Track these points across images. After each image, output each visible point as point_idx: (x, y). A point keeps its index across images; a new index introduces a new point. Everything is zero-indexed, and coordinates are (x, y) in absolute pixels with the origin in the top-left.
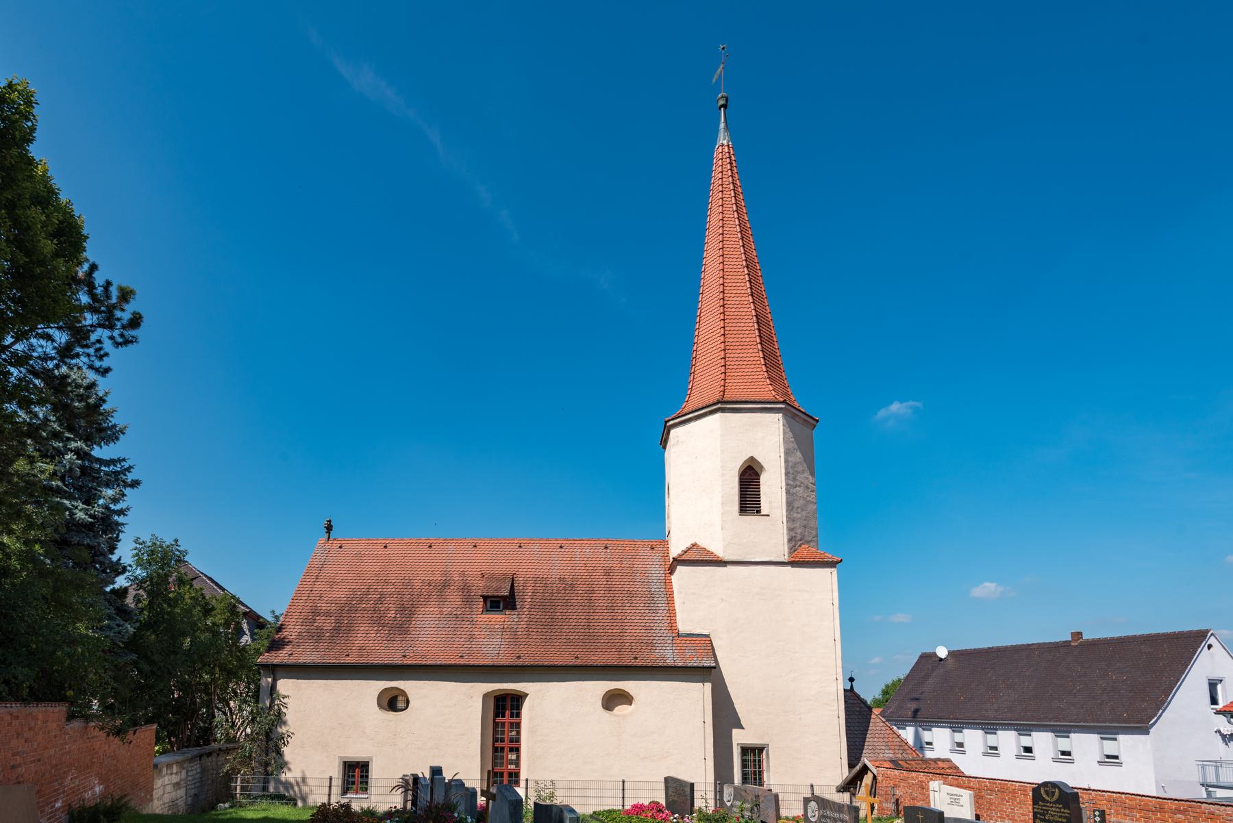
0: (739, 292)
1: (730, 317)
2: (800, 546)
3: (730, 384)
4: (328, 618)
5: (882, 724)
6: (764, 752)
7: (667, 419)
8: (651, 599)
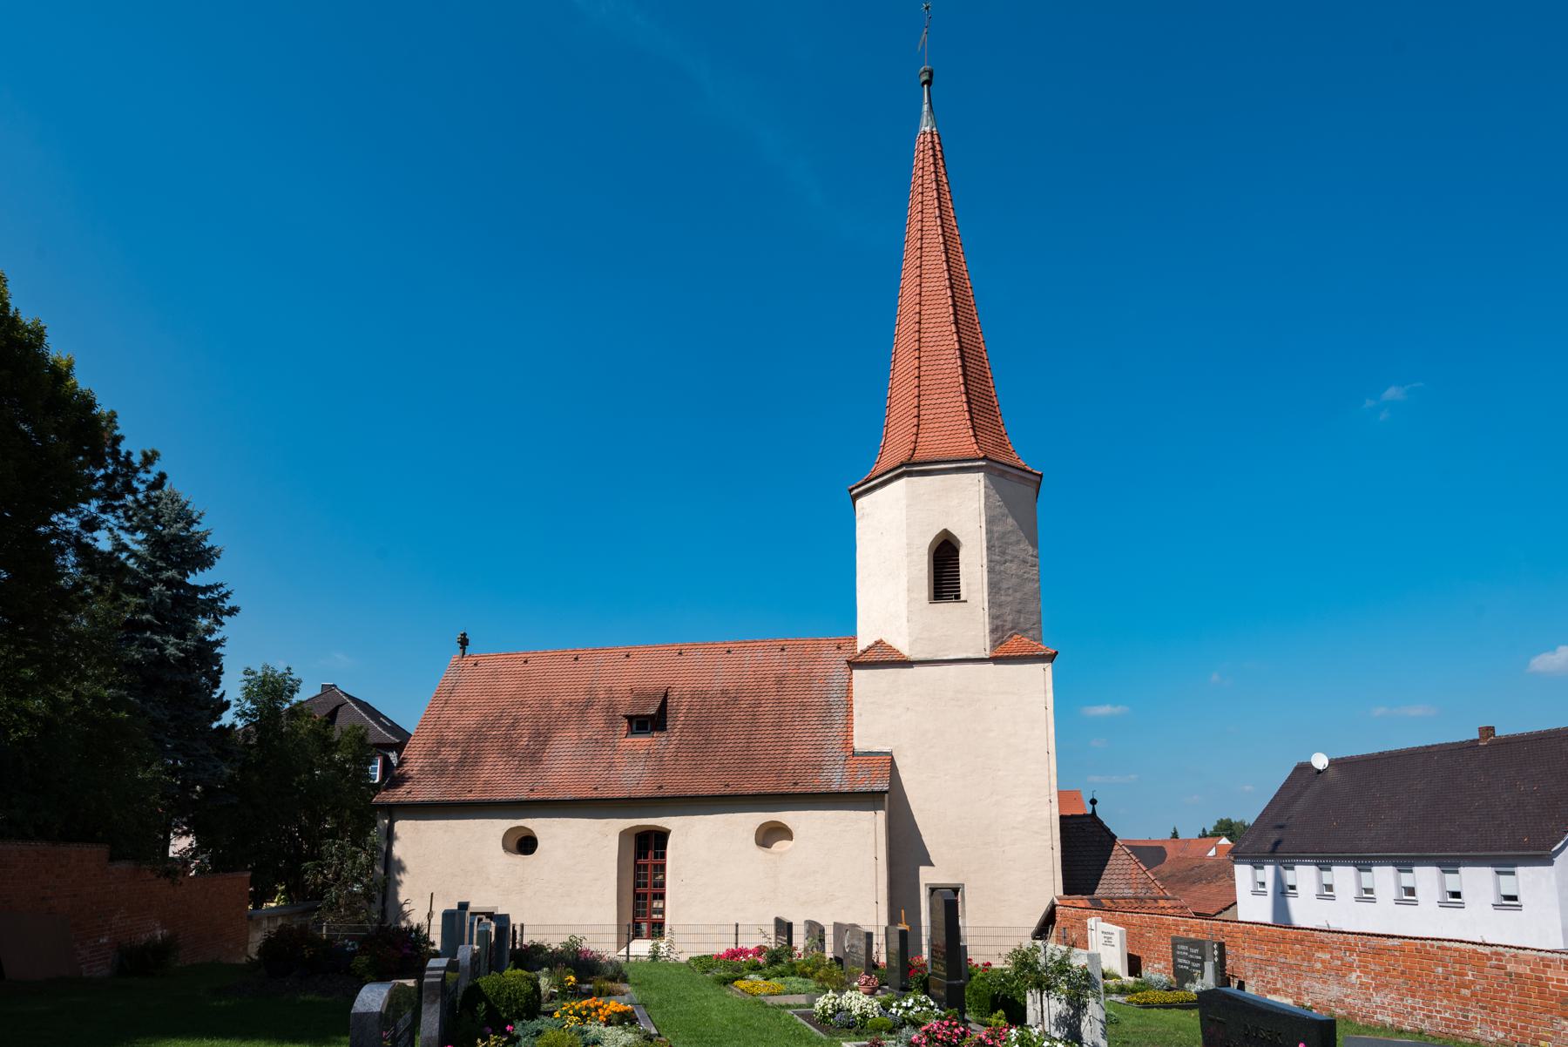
0: (939, 320)
1: (927, 354)
2: (1011, 636)
3: (924, 439)
4: (454, 749)
5: (1126, 857)
6: (959, 893)
7: (850, 487)
8: (827, 711)
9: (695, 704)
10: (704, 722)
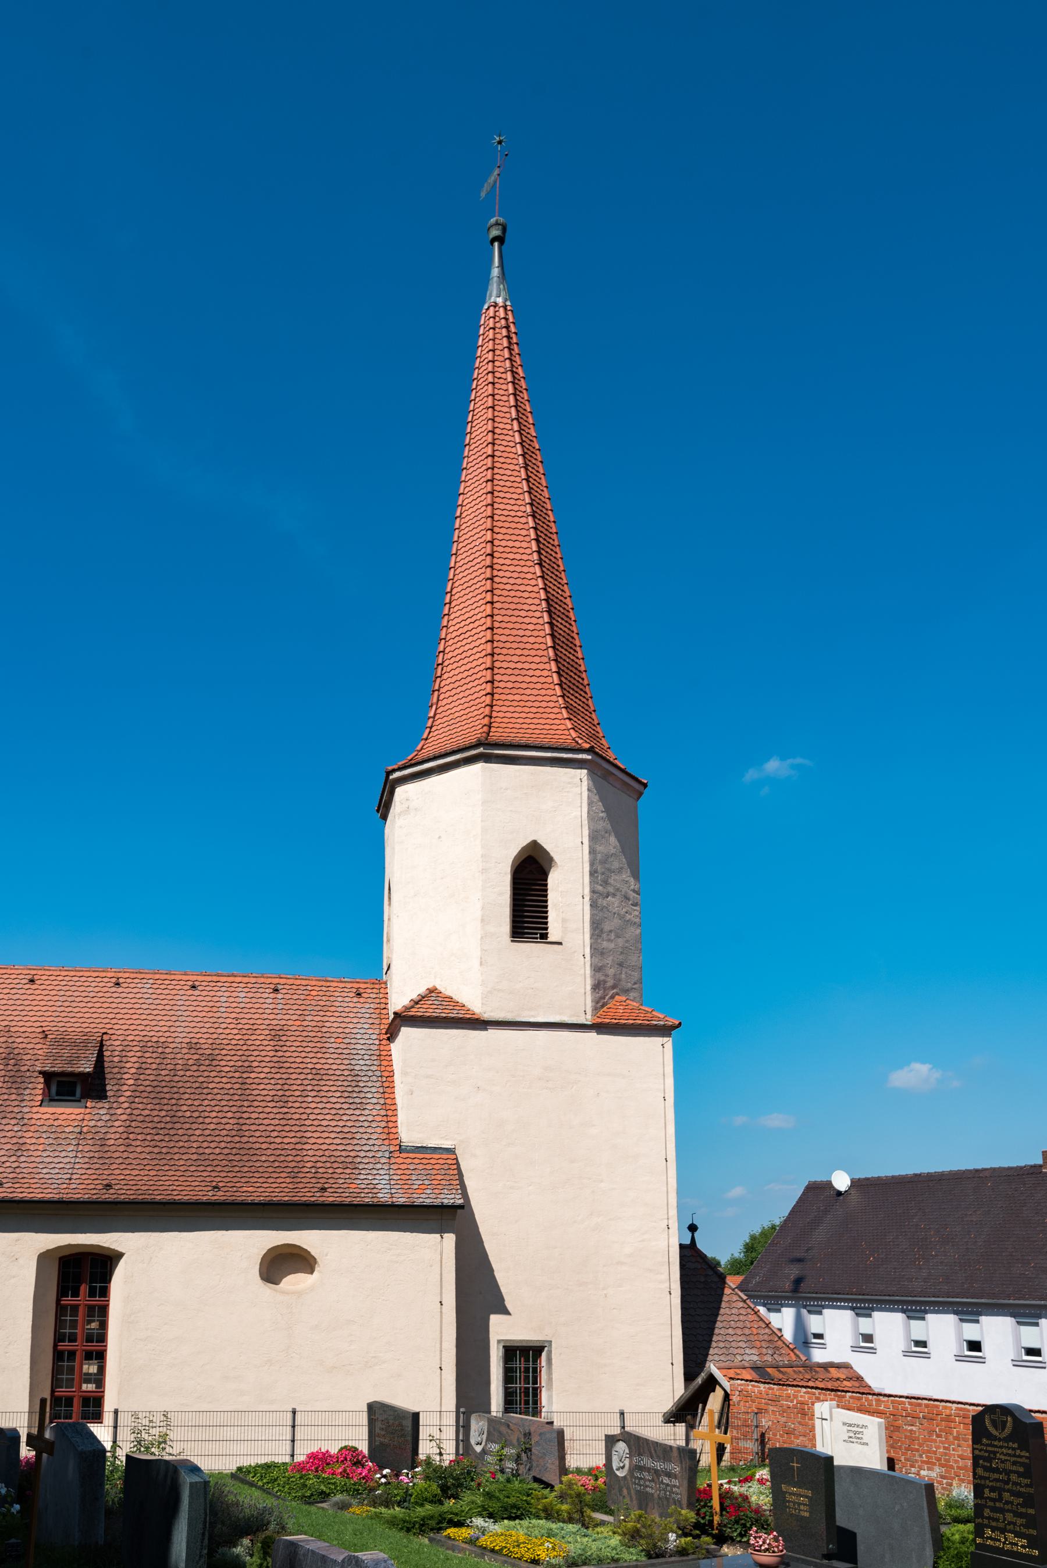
0: (518, 557)
2: (612, 997)
5: (741, 1304)
6: (544, 1354)
7: (390, 768)
9: (149, 1061)
10: (165, 1090)
